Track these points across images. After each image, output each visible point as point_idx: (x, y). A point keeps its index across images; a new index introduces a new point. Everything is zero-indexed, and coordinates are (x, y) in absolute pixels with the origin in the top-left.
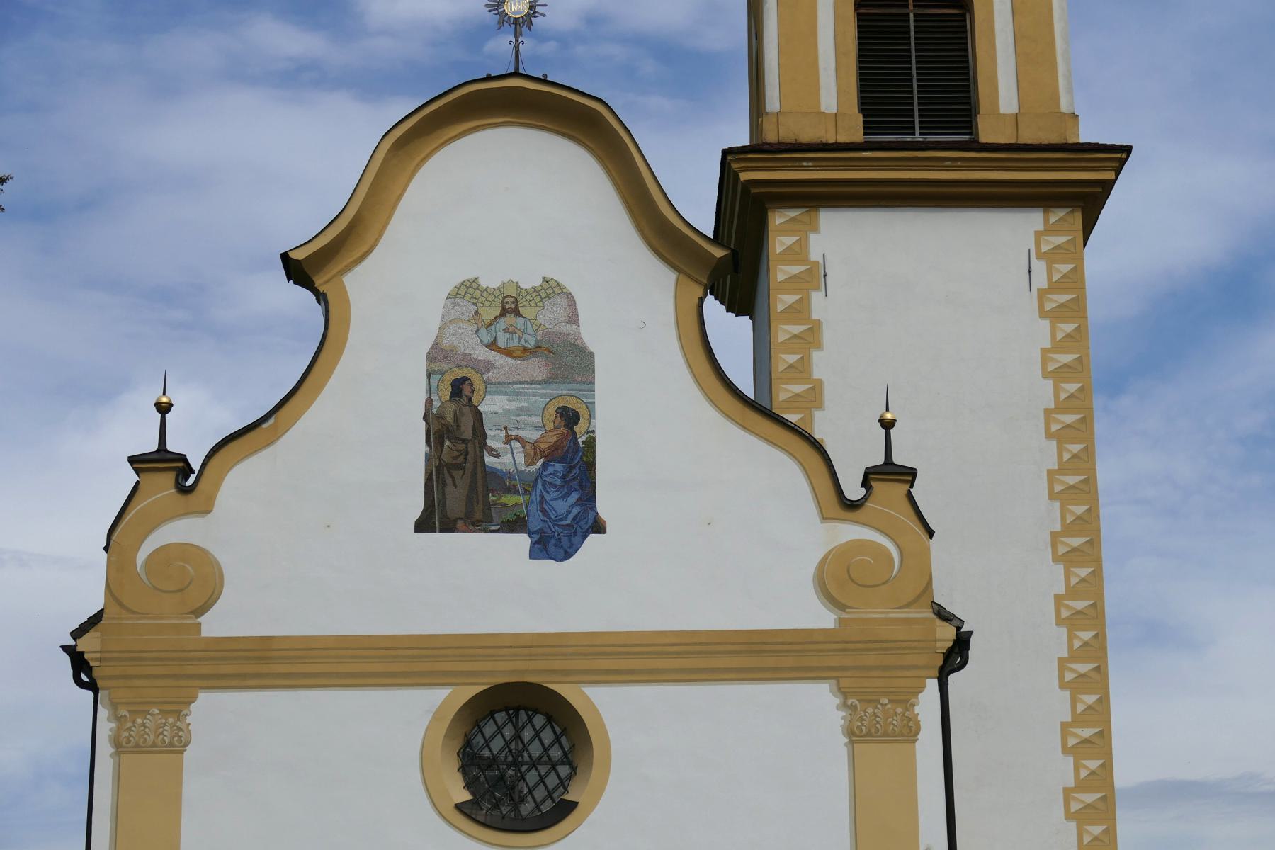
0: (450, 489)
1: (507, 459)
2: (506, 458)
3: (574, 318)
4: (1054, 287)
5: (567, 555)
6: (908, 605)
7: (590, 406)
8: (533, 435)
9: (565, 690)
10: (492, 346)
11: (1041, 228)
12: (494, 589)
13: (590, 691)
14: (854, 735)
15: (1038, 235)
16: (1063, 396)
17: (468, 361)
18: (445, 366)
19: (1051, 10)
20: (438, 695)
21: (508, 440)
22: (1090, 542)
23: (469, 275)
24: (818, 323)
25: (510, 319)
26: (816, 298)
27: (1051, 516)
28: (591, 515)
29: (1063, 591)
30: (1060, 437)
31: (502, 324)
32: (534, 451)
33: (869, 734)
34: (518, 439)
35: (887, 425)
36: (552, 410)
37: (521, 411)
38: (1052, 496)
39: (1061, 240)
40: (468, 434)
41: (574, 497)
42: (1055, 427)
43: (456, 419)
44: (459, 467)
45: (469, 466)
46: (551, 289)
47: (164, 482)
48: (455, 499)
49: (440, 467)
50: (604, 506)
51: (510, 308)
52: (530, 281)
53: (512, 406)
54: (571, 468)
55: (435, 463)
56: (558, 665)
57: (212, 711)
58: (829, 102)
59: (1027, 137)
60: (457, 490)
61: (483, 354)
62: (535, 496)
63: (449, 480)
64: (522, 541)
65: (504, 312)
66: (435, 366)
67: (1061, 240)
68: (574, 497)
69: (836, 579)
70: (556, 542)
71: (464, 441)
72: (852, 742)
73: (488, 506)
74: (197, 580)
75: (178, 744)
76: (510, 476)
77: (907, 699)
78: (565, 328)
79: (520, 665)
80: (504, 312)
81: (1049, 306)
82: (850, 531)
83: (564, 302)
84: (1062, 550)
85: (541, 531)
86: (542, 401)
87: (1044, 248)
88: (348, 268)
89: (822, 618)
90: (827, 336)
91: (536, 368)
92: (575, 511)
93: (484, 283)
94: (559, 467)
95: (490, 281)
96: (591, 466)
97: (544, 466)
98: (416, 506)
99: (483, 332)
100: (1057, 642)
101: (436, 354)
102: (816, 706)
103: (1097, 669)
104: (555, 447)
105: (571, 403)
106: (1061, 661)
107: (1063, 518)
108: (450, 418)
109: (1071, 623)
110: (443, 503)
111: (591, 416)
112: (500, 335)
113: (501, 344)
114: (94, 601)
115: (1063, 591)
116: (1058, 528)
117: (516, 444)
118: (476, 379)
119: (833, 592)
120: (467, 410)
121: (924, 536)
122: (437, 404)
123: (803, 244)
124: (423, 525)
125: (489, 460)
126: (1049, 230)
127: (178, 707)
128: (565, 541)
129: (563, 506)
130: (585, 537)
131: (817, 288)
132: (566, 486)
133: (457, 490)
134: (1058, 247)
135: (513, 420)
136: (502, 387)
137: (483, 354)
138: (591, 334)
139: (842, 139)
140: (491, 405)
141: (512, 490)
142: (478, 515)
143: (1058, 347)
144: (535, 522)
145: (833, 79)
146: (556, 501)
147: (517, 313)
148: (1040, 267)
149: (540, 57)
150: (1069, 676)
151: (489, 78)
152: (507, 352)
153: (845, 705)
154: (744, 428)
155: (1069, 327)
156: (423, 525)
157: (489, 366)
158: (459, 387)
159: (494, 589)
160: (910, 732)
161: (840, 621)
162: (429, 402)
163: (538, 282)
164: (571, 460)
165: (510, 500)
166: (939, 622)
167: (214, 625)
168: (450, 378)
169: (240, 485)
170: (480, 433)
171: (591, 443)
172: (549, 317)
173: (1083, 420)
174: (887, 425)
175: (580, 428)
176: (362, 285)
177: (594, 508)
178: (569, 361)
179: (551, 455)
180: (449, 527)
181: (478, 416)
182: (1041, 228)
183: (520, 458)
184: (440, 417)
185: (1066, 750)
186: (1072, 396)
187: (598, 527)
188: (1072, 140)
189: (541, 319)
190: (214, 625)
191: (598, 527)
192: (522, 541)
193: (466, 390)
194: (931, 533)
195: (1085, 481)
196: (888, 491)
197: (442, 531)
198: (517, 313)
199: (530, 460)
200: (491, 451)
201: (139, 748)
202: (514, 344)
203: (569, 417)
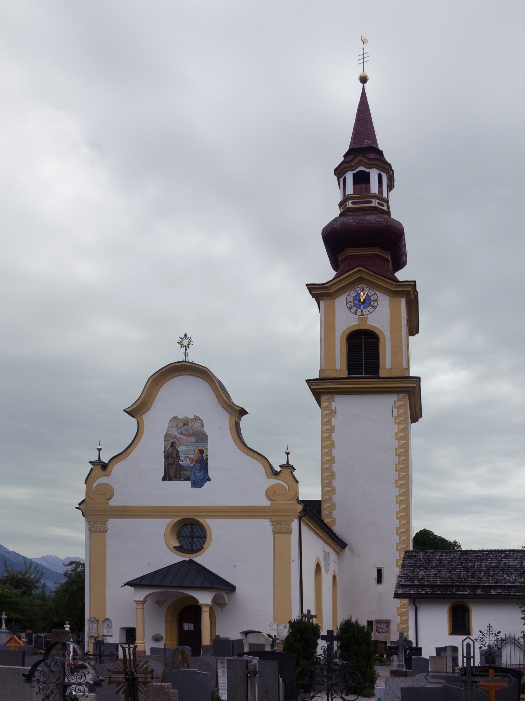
0: (170, 470)
1: (185, 462)
2: (185, 462)
3: (203, 426)
4: (399, 416)
5: (201, 487)
6: (290, 500)
7: (207, 449)
8: (192, 456)
9: (200, 520)
10: (181, 433)
11: (396, 400)
12: (182, 495)
13: (207, 520)
14: (274, 532)
15: (395, 402)
16: (400, 444)
17: (175, 437)
18: (169, 439)
19: (402, 339)
20: (169, 520)
21: (185, 458)
22: (406, 482)
23: (176, 415)
24: (334, 426)
25: (186, 426)
26: (333, 419)
27: (396, 476)
28: (207, 477)
29: (398, 495)
30: (399, 455)
31: (184, 428)
32: (192, 461)
33: (279, 532)
34: (188, 457)
35: (288, 454)
36: (197, 450)
37: (188, 450)
38: (396, 471)
39: (402, 403)
40: (175, 456)
41: (203, 472)
42: (398, 453)
43: (172, 452)
44: (173, 464)
45: (175, 464)
46: (197, 419)
47: (99, 469)
48: (172, 473)
49: (168, 465)
50: (210, 475)
51: (186, 423)
52: (191, 416)
53: (187, 449)
54: (202, 465)
55: (167, 463)
56: (198, 514)
57: (113, 524)
58: (338, 366)
59: (393, 375)
60: (173, 470)
61: (179, 435)
62: (193, 472)
63: (170, 468)
64: (189, 483)
65: (184, 425)
66: (166, 439)
67: (402, 403)
68: (203, 472)
69: (270, 494)
70: (198, 483)
71: (174, 458)
72: (274, 534)
73: (180, 474)
74: (108, 492)
75: (105, 531)
76: (186, 467)
77: (289, 524)
78: (200, 429)
79: (189, 514)
80: (184, 425)
81: (398, 421)
82: (275, 481)
83: (200, 422)
84: (398, 484)
85: (194, 481)
86: (194, 448)
87: (397, 405)
88: (143, 414)
89: (267, 503)
90: (336, 429)
91: (193, 439)
92: (203, 476)
93: (179, 417)
94: (199, 465)
95: (181, 417)
96: (207, 464)
97: (195, 464)
98: (162, 474)
99: (179, 430)
100: (396, 507)
101: (166, 436)
102: (266, 525)
103: (407, 514)
104: (198, 460)
105: (202, 448)
106: (397, 512)
107: (399, 476)
108: (170, 452)
109: (400, 503)
110: (169, 474)
111: (207, 451)
112: (183, 431)
113: (184, 433)
114: (83, 497)
115: (398, 495)
116: (398, 479)
117: (188, 459)
118: (177, 442)
119: (270, 496)
120: (175, 450)
121: (295, 483)
122: (167, 448)
123: (330, 405)
124: (164, 479)
125: (180, 463)
126: (399, 400)
127: (105, 522)
128: (200, 483)
129: (200, 474)
130: (205, 482)
131: (334, 417)
132: (201, 469)
133: (173, 470)
134: (401, 405)
135: (187, 453)
136: (184, 444)
137: (179, 435)
138: (207, 430)
139: (341, 376)
140: (181, 449)
141: (186, 470)
142: (178, 476)
143: (399, 432)
144: (193, 478)
145: (339, 361)
146: (197, 472)
147: (187, 425)
148: (395, 411)
149: (195, 357)
150: (399, 516)
151: (178, 362)
152: (185, 435)
153: (272, 525)
154: (248, 455)
155: (403, 426)
156: (164, 479)
157: (180, 439)
158: (172, 444)
159: (182, 495)
160: (290, 532)
161: (272, 504)
162: (165, 448)
163: (193, 417)
164: (202, 463)
165: (186, 473)
166: (298, 505)
167: (113, 503)
168: (170, 442)
169: (117, 469)
170: (178, 456)
171: (207, 458)
172: (196, 426)
173: (406, 451)
174: (288, 454)
175: (204, 455)
176: (148, 418)
177: (208, 475)
178: (202, 437)
179: (197, 462)
180: (170, 479)
181: (178, 451)
182: (396, 400)
183: (189, 462)
184: (168, 452)
185: (397, 534)
186: (403, 444)
187: (209, 480)
188: (406, 375)
189: (194, 426)
190: (113, 503)
191: (209, 480)
192: (189, 483)
193: (175, 445)
194: (297, 482)
195: (406, 467)
196: (288, 471)
197: (169, 480)
198: (187, 425)
199: (191, 463)
200: (181, 461)
201: (95, 532)
202: (187, 433)
203: (201, 452)
